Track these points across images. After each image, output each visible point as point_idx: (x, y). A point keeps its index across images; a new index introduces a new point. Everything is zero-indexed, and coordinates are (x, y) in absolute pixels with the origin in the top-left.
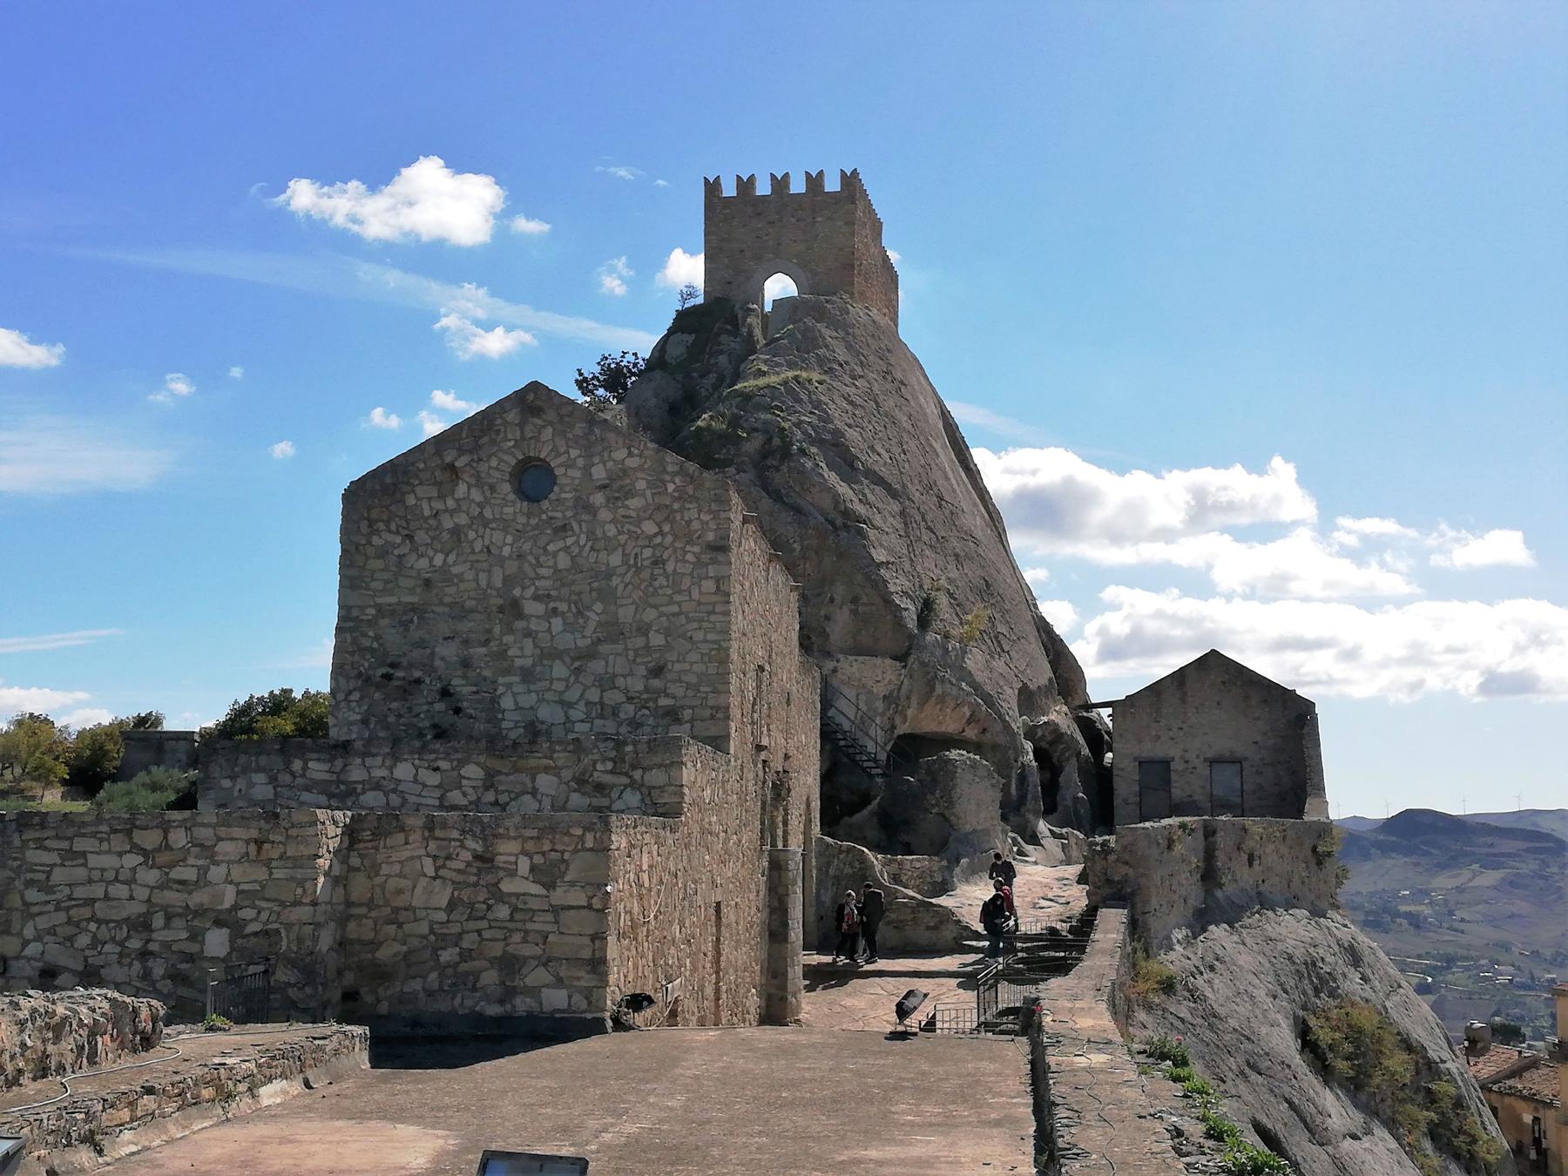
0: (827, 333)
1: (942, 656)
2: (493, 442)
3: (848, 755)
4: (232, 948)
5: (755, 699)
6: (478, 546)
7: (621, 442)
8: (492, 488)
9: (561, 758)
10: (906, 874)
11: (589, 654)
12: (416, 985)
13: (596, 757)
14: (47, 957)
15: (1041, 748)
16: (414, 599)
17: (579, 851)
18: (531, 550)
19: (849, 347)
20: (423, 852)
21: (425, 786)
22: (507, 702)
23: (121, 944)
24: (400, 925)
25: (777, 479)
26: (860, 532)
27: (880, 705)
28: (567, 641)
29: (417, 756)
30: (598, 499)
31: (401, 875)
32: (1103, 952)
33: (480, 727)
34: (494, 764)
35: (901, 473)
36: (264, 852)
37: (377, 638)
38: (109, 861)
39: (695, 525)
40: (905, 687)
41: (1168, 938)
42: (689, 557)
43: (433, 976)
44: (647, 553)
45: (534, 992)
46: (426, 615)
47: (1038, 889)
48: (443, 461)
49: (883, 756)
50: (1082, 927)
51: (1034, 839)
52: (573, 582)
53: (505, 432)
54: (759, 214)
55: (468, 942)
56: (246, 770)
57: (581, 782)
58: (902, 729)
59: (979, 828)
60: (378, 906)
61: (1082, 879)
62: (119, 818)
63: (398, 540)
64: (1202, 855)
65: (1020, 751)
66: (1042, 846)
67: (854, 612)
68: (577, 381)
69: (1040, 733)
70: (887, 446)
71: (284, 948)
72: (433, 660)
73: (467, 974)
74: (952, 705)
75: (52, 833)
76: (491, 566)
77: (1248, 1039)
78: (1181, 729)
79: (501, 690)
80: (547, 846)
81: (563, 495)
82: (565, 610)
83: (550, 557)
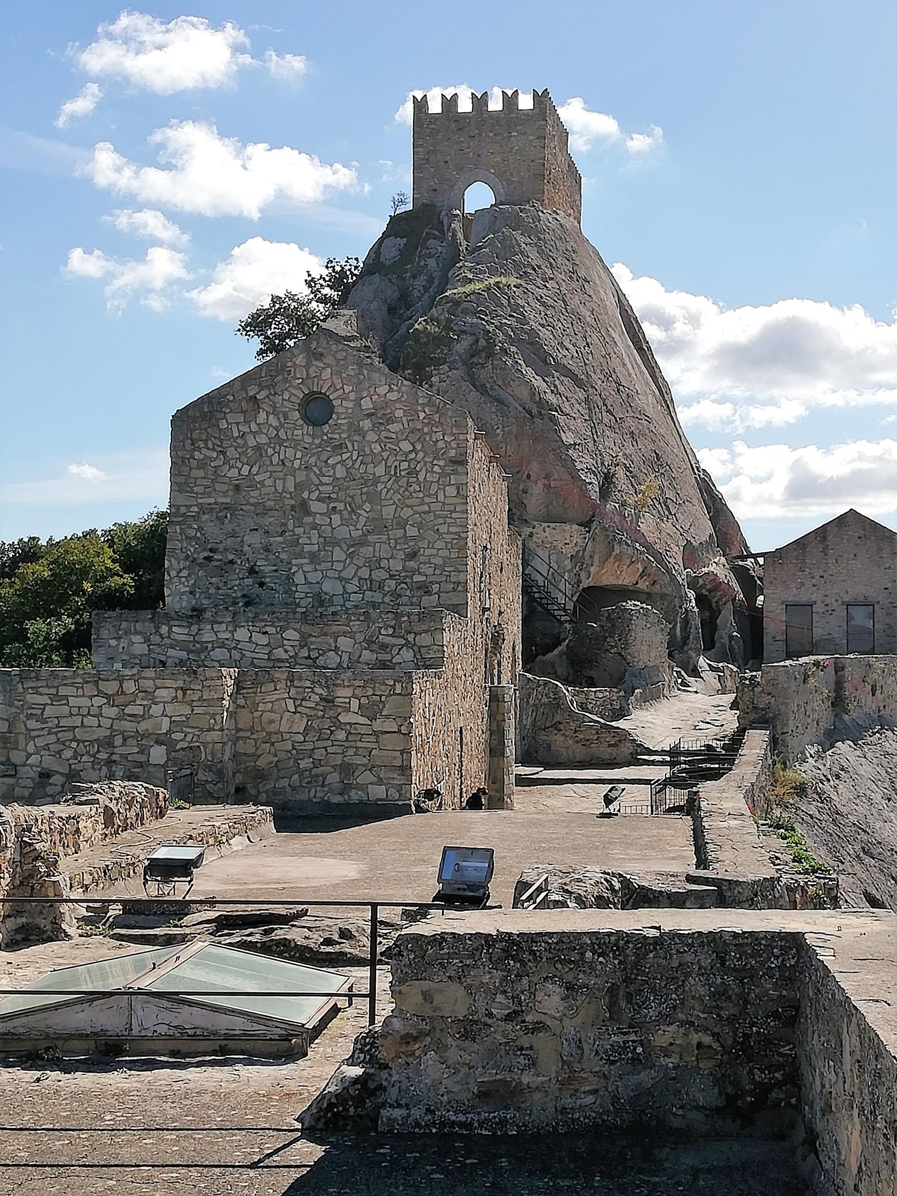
0: (522, 239)
1: (620, 521)
2: (286, 380)
3: (541, 605)
4: (168, 759)
5: (482, 573)
6: (275, 459)
7: (383, 379)
8: (286, 416)
9: (356, 625)
10: (590, 703)
11: (362, 542)
12: (284, 783)
13: (381, 625)
14: (43, 765)
15: (702, 595)
16: (228, 500)
17: (391, 695)
18: (316, 463)
19: (540, 252)
20: (286, 695)
21: (257, 645)
22: (299, 578)
23: (94, 756)
24: (273, 744)
25: (483, 375)
26: (553, 419)
27: (567, 562)
28: (343, 532)
29: (251, 624)
30: (366, 424)
31: (271, 711)
32: (747, 763)
33: (279, 597)
34: (306, 629)
35: (586, 364)
36: (187, 696)
37: (200, 529)
38: (84, 702)
39: (441, 444)
40: (589, 548)
41: (803, 753)
42: (436, 469)
43: (296, 777)
44: (405, 465)
45: (363, 787)
46: (236, 512)
47: (698, 714)
48: (247, 395)
49: (570, 606)
50: (733, 744)
51: (695, 672)
52: (348, 488)
53: (295, 372)
54: (460, 129)
55: (319, 754)
56: (128, 632)
57: (370, 643)
58: (585, 583)
59: (651, 664)
60: (257, 731)
61: (734, 705)
62: (89, 674)
63: (215, 455)
64: (832, 686)
65: (685, 599)
66: (702, 678)
67: (548, 487)
68: (306, 280)
69: (701, 581)
70: (574, 341)
71: (203, 759)
72: (242, 546)
73: (317, 776)
74: (628, 562)
75: (44, 683)
76: (286, 475)
77: (864, 831)
78: (823, 577)
79: (294, 569)
80: (370, 693)
81: (339, 421)
82: (342, 509)
83: (330, 468)
